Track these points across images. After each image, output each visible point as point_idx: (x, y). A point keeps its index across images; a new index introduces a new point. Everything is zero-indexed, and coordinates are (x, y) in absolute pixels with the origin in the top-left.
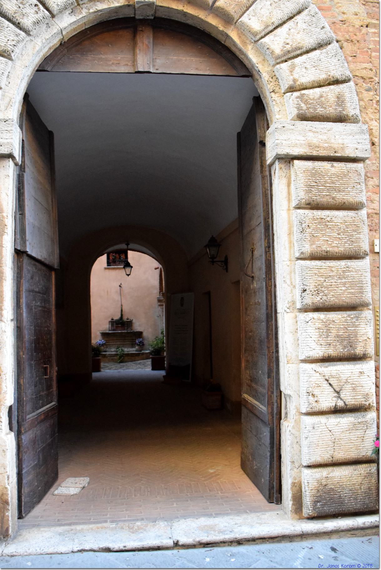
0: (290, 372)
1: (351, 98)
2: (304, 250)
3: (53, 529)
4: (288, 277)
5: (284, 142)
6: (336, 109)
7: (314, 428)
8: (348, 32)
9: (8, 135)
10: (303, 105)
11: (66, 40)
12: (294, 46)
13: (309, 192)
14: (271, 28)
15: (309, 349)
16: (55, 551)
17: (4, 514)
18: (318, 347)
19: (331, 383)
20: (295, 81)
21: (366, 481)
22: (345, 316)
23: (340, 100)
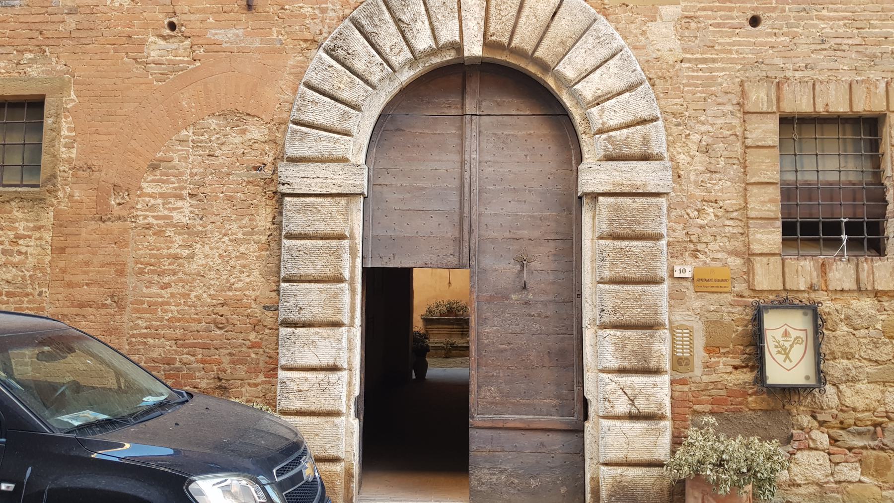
1: (658, 136)
10: (609, 146)
14: (584, 75)
18: (615, 360)
20: (603, 124)
21: (658, 483)
23: (646, 140)
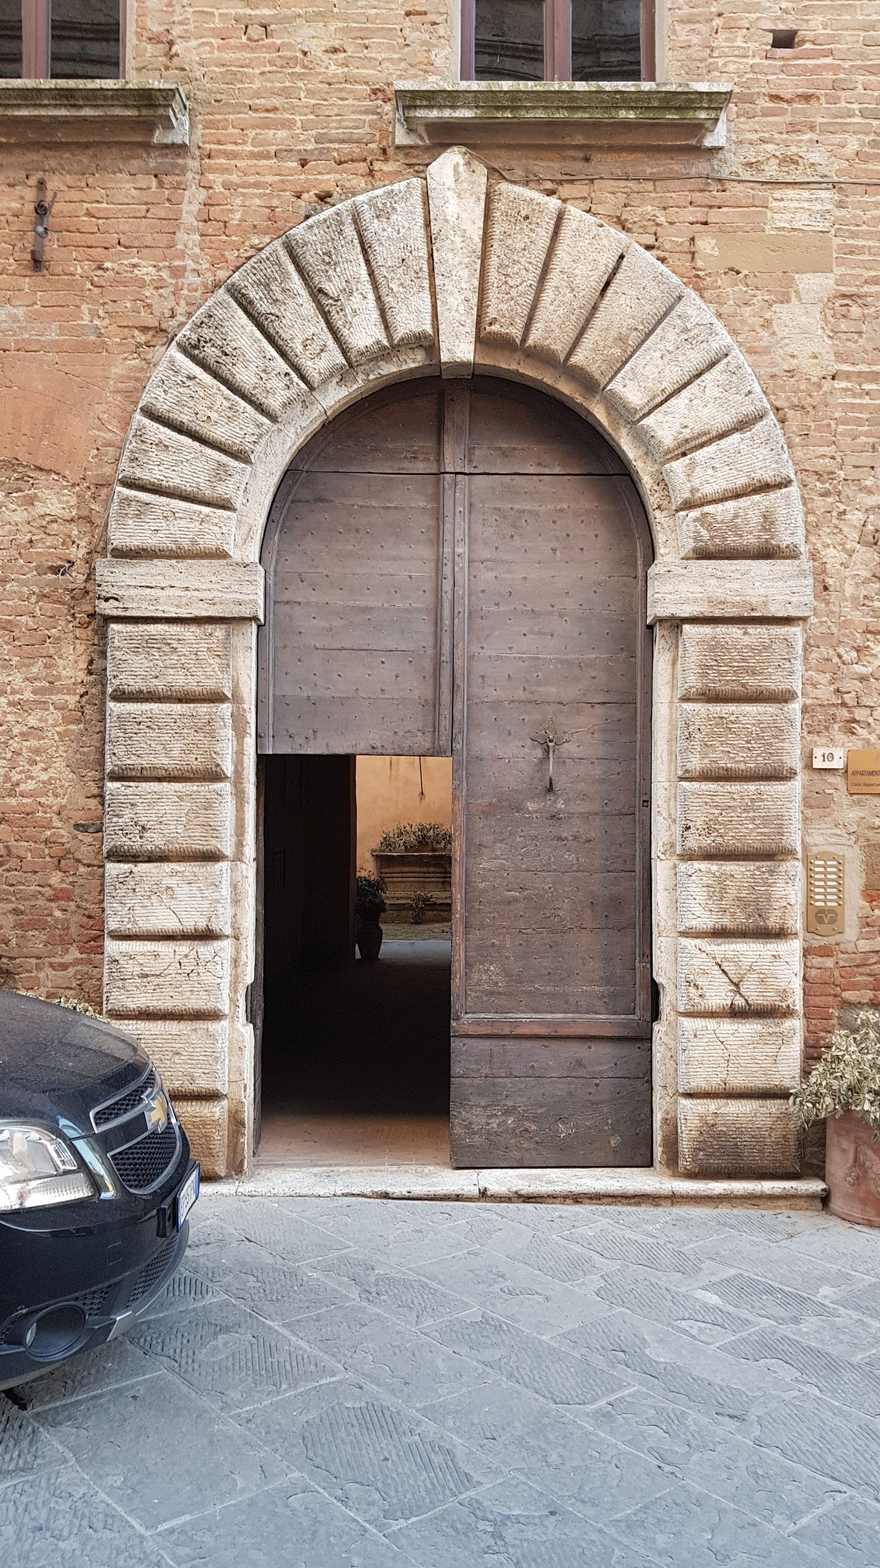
0: (663, 948)
1: (789, 514)
2: (689, 766)
3: (303, 1170)
4: (665, 806)
5: (668, 596)
6: (759, 537)
7: (695, 1036)
8: (796, 391)
9: (251, 587)
10: (704, 532)
11: (331, 418)
12: (697, 429)
13: (705, 675)
14: (659, 400)
15: (690, 916)
16: (310, 1193)
17: (238, 1140)
19: (726, 969)
20: (693, 491)
21: (780, 1125)
22: (752, 868)
23: (768, 521)
